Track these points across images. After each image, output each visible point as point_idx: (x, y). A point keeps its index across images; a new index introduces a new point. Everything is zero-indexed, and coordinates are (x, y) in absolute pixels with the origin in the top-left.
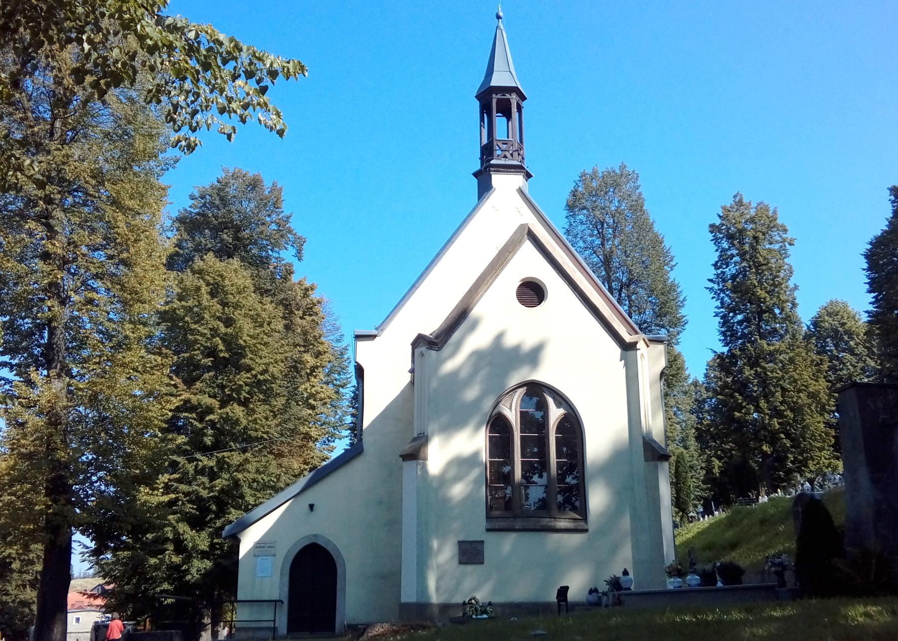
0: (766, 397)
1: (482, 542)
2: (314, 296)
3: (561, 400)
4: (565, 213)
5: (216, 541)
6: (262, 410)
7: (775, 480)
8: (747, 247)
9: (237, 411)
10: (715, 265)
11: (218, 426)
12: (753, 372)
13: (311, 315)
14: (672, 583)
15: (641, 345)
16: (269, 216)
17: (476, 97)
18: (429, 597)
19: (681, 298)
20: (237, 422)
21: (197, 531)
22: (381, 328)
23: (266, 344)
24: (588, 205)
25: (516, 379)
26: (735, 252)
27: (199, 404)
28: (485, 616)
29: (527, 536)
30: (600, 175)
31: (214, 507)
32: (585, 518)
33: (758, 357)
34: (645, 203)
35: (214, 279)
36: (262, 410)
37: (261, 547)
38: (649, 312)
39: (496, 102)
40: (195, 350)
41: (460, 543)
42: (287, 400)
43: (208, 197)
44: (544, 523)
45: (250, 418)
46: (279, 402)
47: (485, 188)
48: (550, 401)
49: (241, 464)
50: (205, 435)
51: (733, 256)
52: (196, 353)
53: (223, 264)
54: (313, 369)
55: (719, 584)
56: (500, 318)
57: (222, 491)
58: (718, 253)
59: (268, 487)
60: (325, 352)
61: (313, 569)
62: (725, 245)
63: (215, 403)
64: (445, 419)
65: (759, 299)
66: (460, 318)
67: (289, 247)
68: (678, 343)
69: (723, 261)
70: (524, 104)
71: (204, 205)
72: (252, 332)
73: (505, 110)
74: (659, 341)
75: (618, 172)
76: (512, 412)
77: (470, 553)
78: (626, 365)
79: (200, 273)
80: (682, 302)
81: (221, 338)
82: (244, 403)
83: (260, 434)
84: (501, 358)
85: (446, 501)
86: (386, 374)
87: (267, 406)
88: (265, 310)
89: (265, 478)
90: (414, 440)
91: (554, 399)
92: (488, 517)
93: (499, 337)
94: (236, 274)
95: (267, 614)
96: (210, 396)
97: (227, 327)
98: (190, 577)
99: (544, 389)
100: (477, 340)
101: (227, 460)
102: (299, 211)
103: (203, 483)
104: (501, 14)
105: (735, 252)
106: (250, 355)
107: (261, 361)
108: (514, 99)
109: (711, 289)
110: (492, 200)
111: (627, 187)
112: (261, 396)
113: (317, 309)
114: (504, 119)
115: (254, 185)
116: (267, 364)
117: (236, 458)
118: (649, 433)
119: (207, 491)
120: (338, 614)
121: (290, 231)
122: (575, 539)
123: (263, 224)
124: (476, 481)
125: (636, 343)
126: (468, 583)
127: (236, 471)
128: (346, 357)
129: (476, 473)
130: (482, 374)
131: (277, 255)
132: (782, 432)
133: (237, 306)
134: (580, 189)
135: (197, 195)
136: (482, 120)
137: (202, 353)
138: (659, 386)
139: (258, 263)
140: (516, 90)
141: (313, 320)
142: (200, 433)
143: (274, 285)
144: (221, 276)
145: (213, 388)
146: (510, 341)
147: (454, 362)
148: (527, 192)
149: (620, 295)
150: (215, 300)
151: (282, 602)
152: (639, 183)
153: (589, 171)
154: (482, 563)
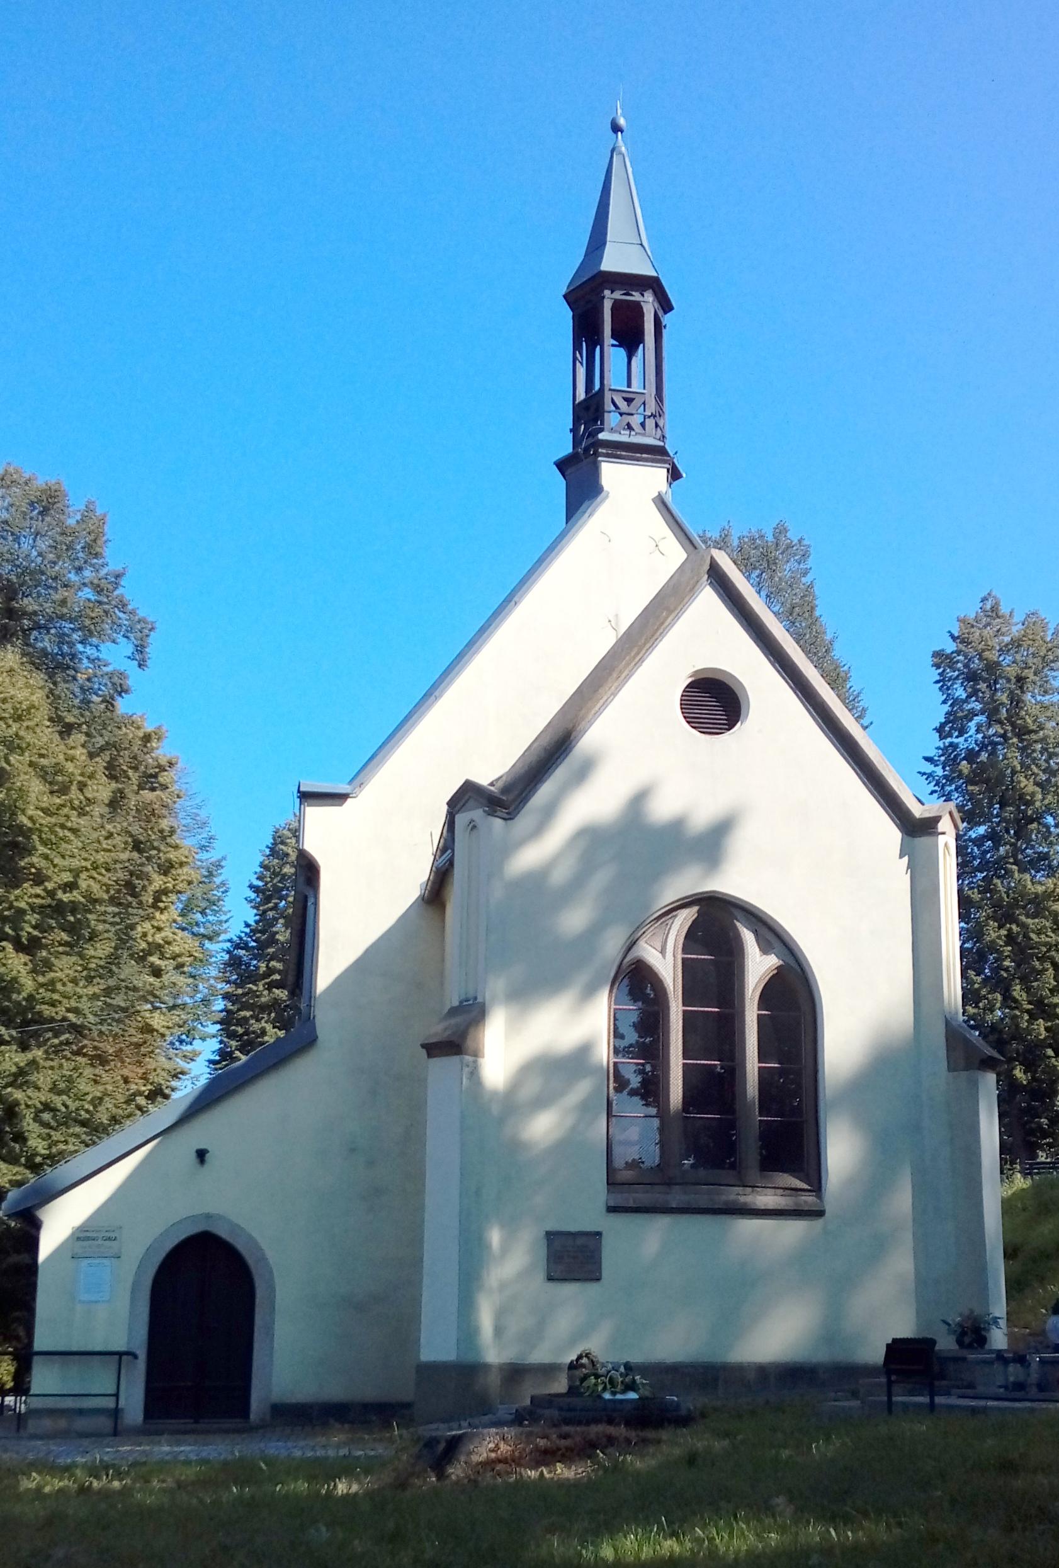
0: (1025, 980)
1: (599, 1234)
2: (162, 751)
3: (772, 935)
6: (65, 966)
7: (1032, 1132)
8: (1003, 697)
10: (940, 730)
12: (1003, 932)
13: (153, 789)
17: (565, 297)
23: (74, 831)
26: (978, 706)
28: (632, 1395)
29: (684, 1220)
33: (1015, 904)
36: (65, 966)
39: (608, 311)
41: (551, 1236)
42: (116, 948)
44: (732, 1197)
45: (41, 979)
46: (100, 950)
48: (748, 938)
49: (21, 1072)
51: (972, 714)
56: (641, 753)
58: (946, 708)
59: (76, 1121)
61: (202, 1293)
62: (960, 693)
65: (1021, 797)
66: (554, 753)
67: (121, 639)
69: (953, 723)
70: (666, 319)
72: (46, 801)
73: (629, 337)
76: (665, 960)
77: (572, 1257)
82: (28, 947)
83: (61, 1012)
84: (641, 843)
85: (516, 1146)
88: (72, 759)
89: (69, 1102)
90: (453, 1012)
91: (756, 933)
93: (639, 800)
95: (101, 1381)
99: (737, 913)
102: (142, 563)
104: (622, 122)
105: (978, 706)
106: (42, 849)
107: (66, 863)
108: (648, 302)
109: (929, 776)
110: (599, 520)
112: (65, 936)
114: (622, 352)
116: (76, 872)
120: (255, 1382)
121: (122, 605)
122: (793, 1230)
124: (584, 1107)
125: (937, 819)
128: (218, 880)
129: (582, 1089)
132: (1050, 1046)
140: (652, 284)
146: (663, 808)
147: (542, 847)
151: (135, 1357)
152: (810, 563)
154: (598, 1279)
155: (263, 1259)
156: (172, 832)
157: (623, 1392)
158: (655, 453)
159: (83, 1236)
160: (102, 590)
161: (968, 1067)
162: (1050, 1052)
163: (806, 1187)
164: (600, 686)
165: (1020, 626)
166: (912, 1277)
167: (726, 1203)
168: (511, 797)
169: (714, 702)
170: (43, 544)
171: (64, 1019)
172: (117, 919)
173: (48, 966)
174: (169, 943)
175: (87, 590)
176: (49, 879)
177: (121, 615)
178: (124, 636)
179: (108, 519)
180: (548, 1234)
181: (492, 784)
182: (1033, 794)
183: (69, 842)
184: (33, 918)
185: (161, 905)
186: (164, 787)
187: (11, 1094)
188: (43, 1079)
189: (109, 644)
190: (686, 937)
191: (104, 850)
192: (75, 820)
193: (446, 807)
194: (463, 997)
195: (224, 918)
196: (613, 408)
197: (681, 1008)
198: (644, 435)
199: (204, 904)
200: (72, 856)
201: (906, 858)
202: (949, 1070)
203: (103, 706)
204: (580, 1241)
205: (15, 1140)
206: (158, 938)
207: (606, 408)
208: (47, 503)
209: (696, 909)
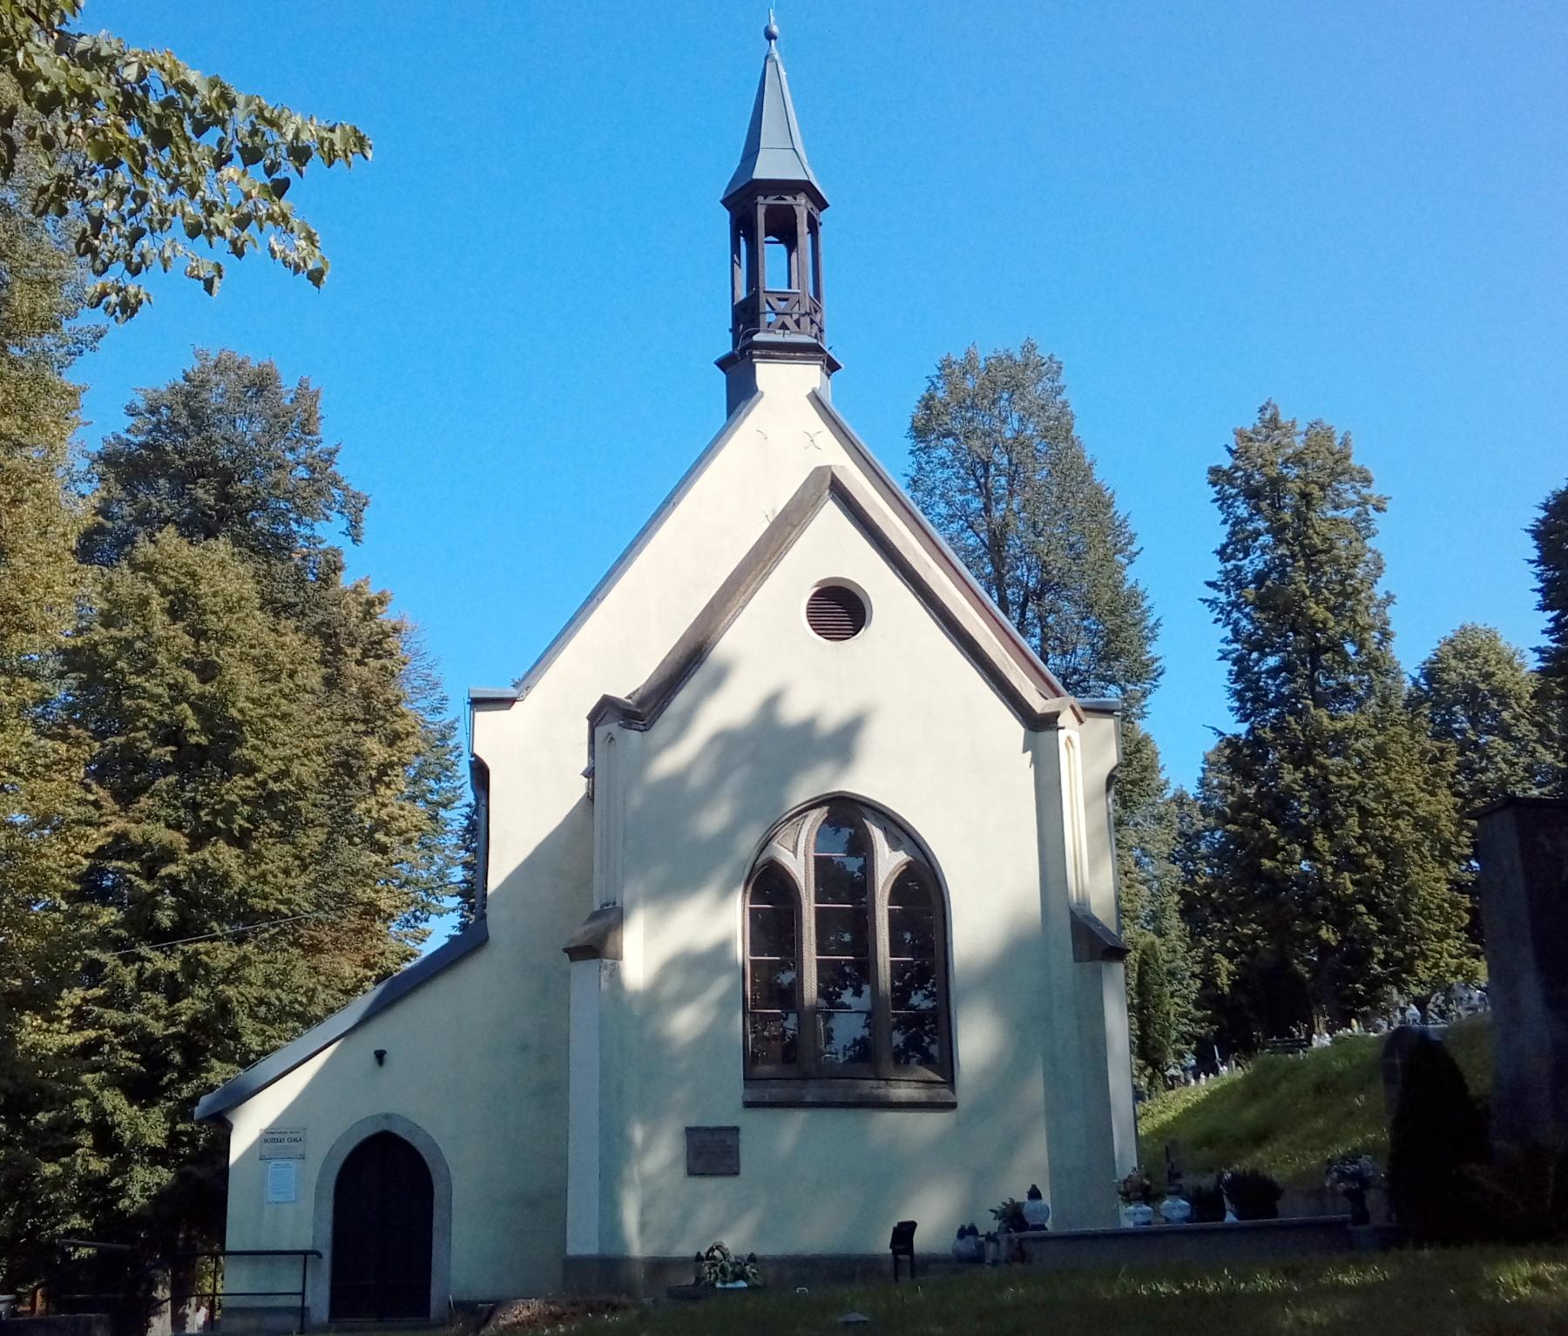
0: (1327, 827)
1: (736, 1130)
2: (387, 616)
3: (901, 833)
4: (909, 444)
5: (180, 1127)
6: (276, 855)
8: (1287, 515)
9: (226, 857)
10: (1222, 553)
11: (186, 888)
12: (1299, 775)
13: (378, 657)
15: (1066, 719)
16: (292, 449)
17: (724, 202)
18: (624, 1244)
21: (142, 1107)
22: (525, 683)
23: (285, 717)
24: (957, 426)
26: (1262, 525)
27: (146, 841)
29: (828, 1115)
30: (982, 365)
31: (177, 1058)
32: (950, 1080)
33: (1310, 744)
35: (178, 582)
36: (276, 855)
37: (274, 1140)
39: (765, 213)
40: (137, 730)
41: (690, 1132)
42: (329, 833)
43: (164, 411)
44: (866, 1091)
45: (252, 872)
46: (313, 839)
47: (741, 391)
48: (877, 835)
49: (233, 968)
50: (158, 906)
51: (1257, 534)
52: (140, 735)
53: (197, 550)
54: (384, 769)
55: (1230, 1218)
56: (773, 658)
57: (194, 1023)
58: (1227, 528)
59: (289, 1014)
60: (408, 734)
61: (384, 1186)
62: (1242, 511)
65: (1313, 622)
66: (690, 662)
67: (334, 515)
68: (1143, 716)
69: (1237, 544)
70: (823, 217)
72: (256, 692)
74: (1106, 711)
75: (1018, 357)
76: (797, 858)
77: (711, 1153)
78: (1035, 761)
79: (148, 569)
80: (1152, 630)
81: (191, 705)
82: (240, 841)
83: (272, 904)
85: (660, 1043)
89: (283, 996)
90: (595, 916)
91: (885, 830)
92: (748, 1078)
93: (771, 703)
94: (221, 569)
95: (287, 1280)
96: (168, 826)
97: (203, 681)
98: (127, 1202)
99: (865, 810)
100: (725, 709)
102: (354, 440)
103: (155, 1007)
104: (775, 29)
105: (1262, 525)
106: (252, 741)
108: (802, 205)
109: (1212, 603)
110: (756, 418)
111: (1036, 391)
112: (275, 826)
113: (391, 643)
114: (782, 248)
116: (288, 760)
117: (223, 955)
118: (1084, 903)
119: (162, 1023)
120: (434, 1279)
121: (335, 482)
122: (931, 1123)
123: (279, 467)
124: (723, 1004)
125: (1057, 715)
127: (224, 981)
129: (722, 985)
130: (736, 780)
131: (307, 531)
132: (1360, 901)
133: (225, 638)
134: (940, 394)
135: (142, 405)
136: (735, 249)
137: (153, 736)
139: (271, 548)
140: (805, 188)
141: (384, 668)
144: (193, 575)
145: (176, 808)
146: (795, 710)
147: (679, 753)
148: (828, 399)
149: (1023, 615)
151: (319, 1255)
152: (1062, 381)
154: (736, 1173)
155: (439, 1156)
157: (734, 1281)
158: (810, 352)
159: (271, 1137)
162: (1362, 908)
165: (1303, 437)
167: (861, 1096)
168: (646, 709)
169: (840, 610)
170: (257, 428)
172: (334, 802)
173: (259, 857)
175: (300, 468)
176: (259, 769)
179: (321, 395)
181: (629, 697)
182: (1324, 623)
183: (279, 731)
184: (246, 809)
185: (386, 779)
187: (223, 991)
188: (254, 973)
192: (285, 706)
193: (586, 723)
195: (458, 784)
196: (768, 309)
197: (814, 905)
199: (438, 770)
200: (284, 745)
201: (1029, 753)
205: (230, 1037)
206: (384, 814)
208: (261, 385)
209: (826, 809)
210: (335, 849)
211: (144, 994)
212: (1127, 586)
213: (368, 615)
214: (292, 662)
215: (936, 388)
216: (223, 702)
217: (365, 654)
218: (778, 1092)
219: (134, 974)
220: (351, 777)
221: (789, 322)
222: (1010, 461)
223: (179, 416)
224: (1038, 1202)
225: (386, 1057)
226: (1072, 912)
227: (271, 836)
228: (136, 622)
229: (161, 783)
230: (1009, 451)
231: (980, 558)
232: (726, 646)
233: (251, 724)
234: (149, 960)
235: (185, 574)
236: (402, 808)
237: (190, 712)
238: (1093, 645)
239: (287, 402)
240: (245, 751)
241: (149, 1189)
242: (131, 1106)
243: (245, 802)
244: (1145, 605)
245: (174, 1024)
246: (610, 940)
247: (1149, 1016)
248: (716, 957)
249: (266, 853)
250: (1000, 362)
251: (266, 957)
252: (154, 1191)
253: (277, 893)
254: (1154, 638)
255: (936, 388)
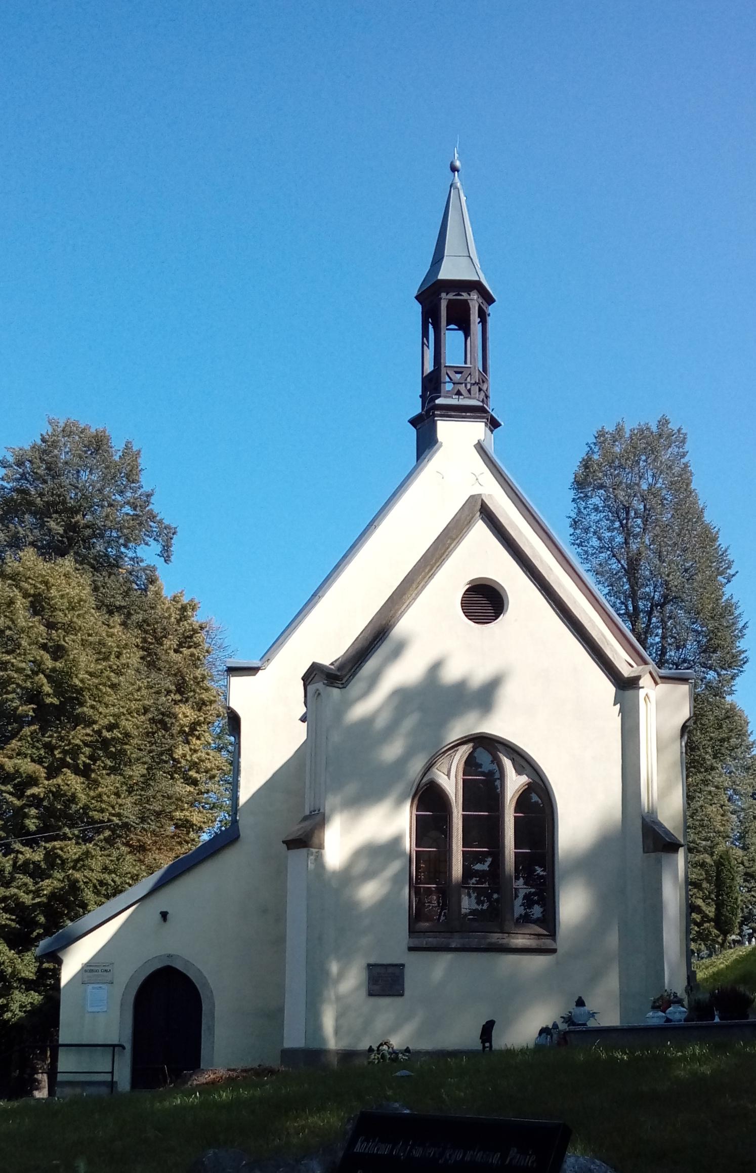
1: (403, 965)
2: (197, 618)
3: (524, 762)
4: (572, 494)
5: (45, 965)
9: (73, 782)
11: (45, 803)
13: (189, 647)
14: (654, 1018)
15: (646, 681)
16: (121, 493)
17: (417, 298)
18: (323, 1039)
19: (740, 625)
20: (73, 799)
21: (19, 952)
22: (267, 657)
23: (113, 686)
24: (608, 482)
25: (458, 730)
27: (17, 771)
30: (627, 435)
31: (42, 919)
32: (553, 934)
34: (694, 478)
35: (35, 587)
36: (109, 783)
37: (92, 971)
38: (691, 645)
39: (448, 305)
40: (8, 693)
41: (370, 967)
43: (28, 464)
44: (493, 940)
45: (92, 793)
46: (137, 771)
47: (426, 442)
48: (508, 764)
50: (26, 816)
52: (10, 696)
53: (48, 565)
54: (194, 726)
55: (717, 1020)
56: (437, 638)
57: (52, 896)
60: (211, 702)
61: (167, 1005)
63: (42, 772)
64: (351, 788)
66: (377, 639)
67: (151, 541)
68: (731, 693)
70: (491, 309)
71: (23, 476)
72: (93, 667)
74: (683, 680)
75: (654, 429)
76: (450, 781)
77: (385, 981)
79: (15, 578)
80: (741, 631)
81: (46, 676)
82: (84, 772)
84: (439, 699)
85: (352, 905)
86: (270, 725)
87: (119, 778)
88: (111, 635)
89: (117, 879)
90: (306, 818)
91: (513, 760)
92: (412, 931)
93: (435, 668)
94: (67, 580)
95: (101, 1064)
96: (33, 761)
97: (55, 659)
98: (9, 1014)
99: (500, 747)
100: (404, 672)
101: (59, 852)
102: (165, 487)
103: (25, 884)
104: (458, 164)
106: (90, 702)
108: (474, 300)
110: (437, 461)
111: (666, 456)
112: (109, 763)
113: (199, 637)
114: (461, 334)
115: (97, 445)
116: (117, 716)
117: (73, 850)
118: (652, 813)
119: (31, 896)
121: (152, 517)
122: (541, 961)
123: (110, 505)
124: (395, 879)
125: (638, 678)
126: (381, 1023)
127: (74, 868)
129: (395, 866)
130: (409, 723)
131: (131, 554)
133: (70, 628)
134: (596, 457)
135: (11, 460)
136: (425, 334)
137: (21, 698)
138: (676, 749)
139: (104, 565)
140: (477, 286)
141: (192, 655)
142: (20, 814)
143: (131, 603)
144: (46, 583)
145: (38, 749)
146: (452, 673)
147: (369, 704)
148: (491, 450)
149: (650, 620)
150: (37, 618)
151: (124, 1048)
153: (610, 428)
154: (402, 995)
155: (206, 984)
156: (204, 678)
159: (89, 969)
160: (136, 506)
161: (656, 850)
163: (546, 933)
164: (405, 594)
166: (618, 993)
167: (490, 944)
169: (484, 601)
171: (109, 820)
173: (96, 783)
174: (203, 761)
177: (152, 524)
178: (154, 539)
179: (142, 452)
180: (369, 965)
181: (332, 664)
183: (109, 695)
184: (87, 750)
185: (197, 733)
186: (197, 645)
189: (143, 546)
190: (466, 762)
191: (136, 700)
194: (312, 809)
196: (448, 379)
197: (461, 812)
198: (470, 398)
200: (113, 705)
201: (618, 706)
202: (644, 852)
203: (139, 592)
204: (390, 970)
207: (442, 380)
209: (471, 745)
210: (155, 780)
211: (17, 876)
212: (724, 598)
213: (183, 618)
214: (118, 646)
215: (593, 452)
216: (69, 675)
217: (180, 645)
218: (432, 941)
219: (11, 862)
220: (166, 731)
221: (462, 388)
222: (645, 506)
223: (39, 468)
224: (582, 1008)
225: (168, 916)
226: (643, 819)
227: (104, 768)
228: (5, 616)
229: (27, 730)
230: (644, 499)
231: (620, 578)
232: (404, 626)
233: (89, 689)
234: (22, 853)
235: (41, 583)
236: (208, 754)
237: (45, 681)
238: (699, 642)
239: (117, 458)
240: (85, 709)
241: (25, 1006)
242: (10, 950)
243: (86, 745)
244: (737, 612)
245: (39, 896)
246: (316, 835)
247: (723, 900)
248: (392, 847)
249: (101, 781)
250: (642, 433)
251: (106, 852)
252: (29, 1008)
253: (110, 809)
254: (742, 637)
255: (593, 452)
